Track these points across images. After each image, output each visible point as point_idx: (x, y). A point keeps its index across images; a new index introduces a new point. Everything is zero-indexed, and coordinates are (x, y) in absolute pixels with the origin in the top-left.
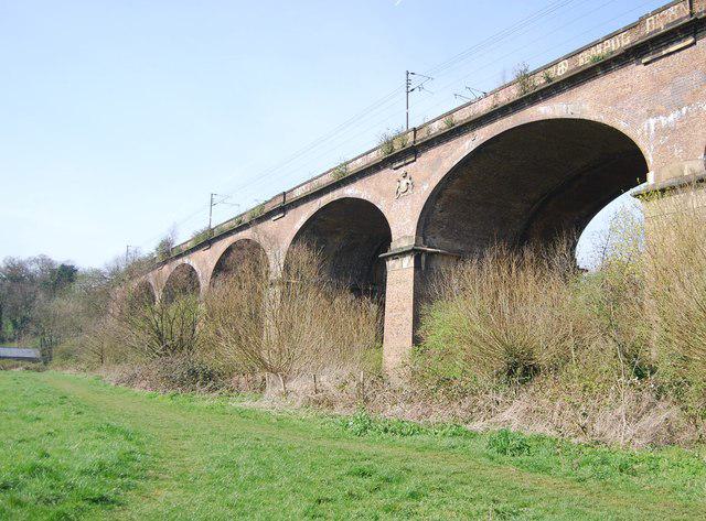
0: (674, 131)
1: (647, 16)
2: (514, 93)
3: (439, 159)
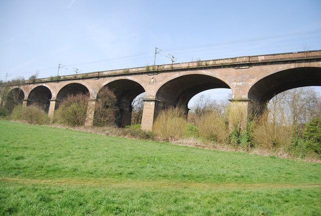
0: (241, 87)
2: (195, 65)
3: (166, 76)
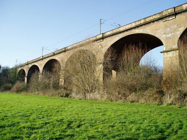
1: (164, 11)
